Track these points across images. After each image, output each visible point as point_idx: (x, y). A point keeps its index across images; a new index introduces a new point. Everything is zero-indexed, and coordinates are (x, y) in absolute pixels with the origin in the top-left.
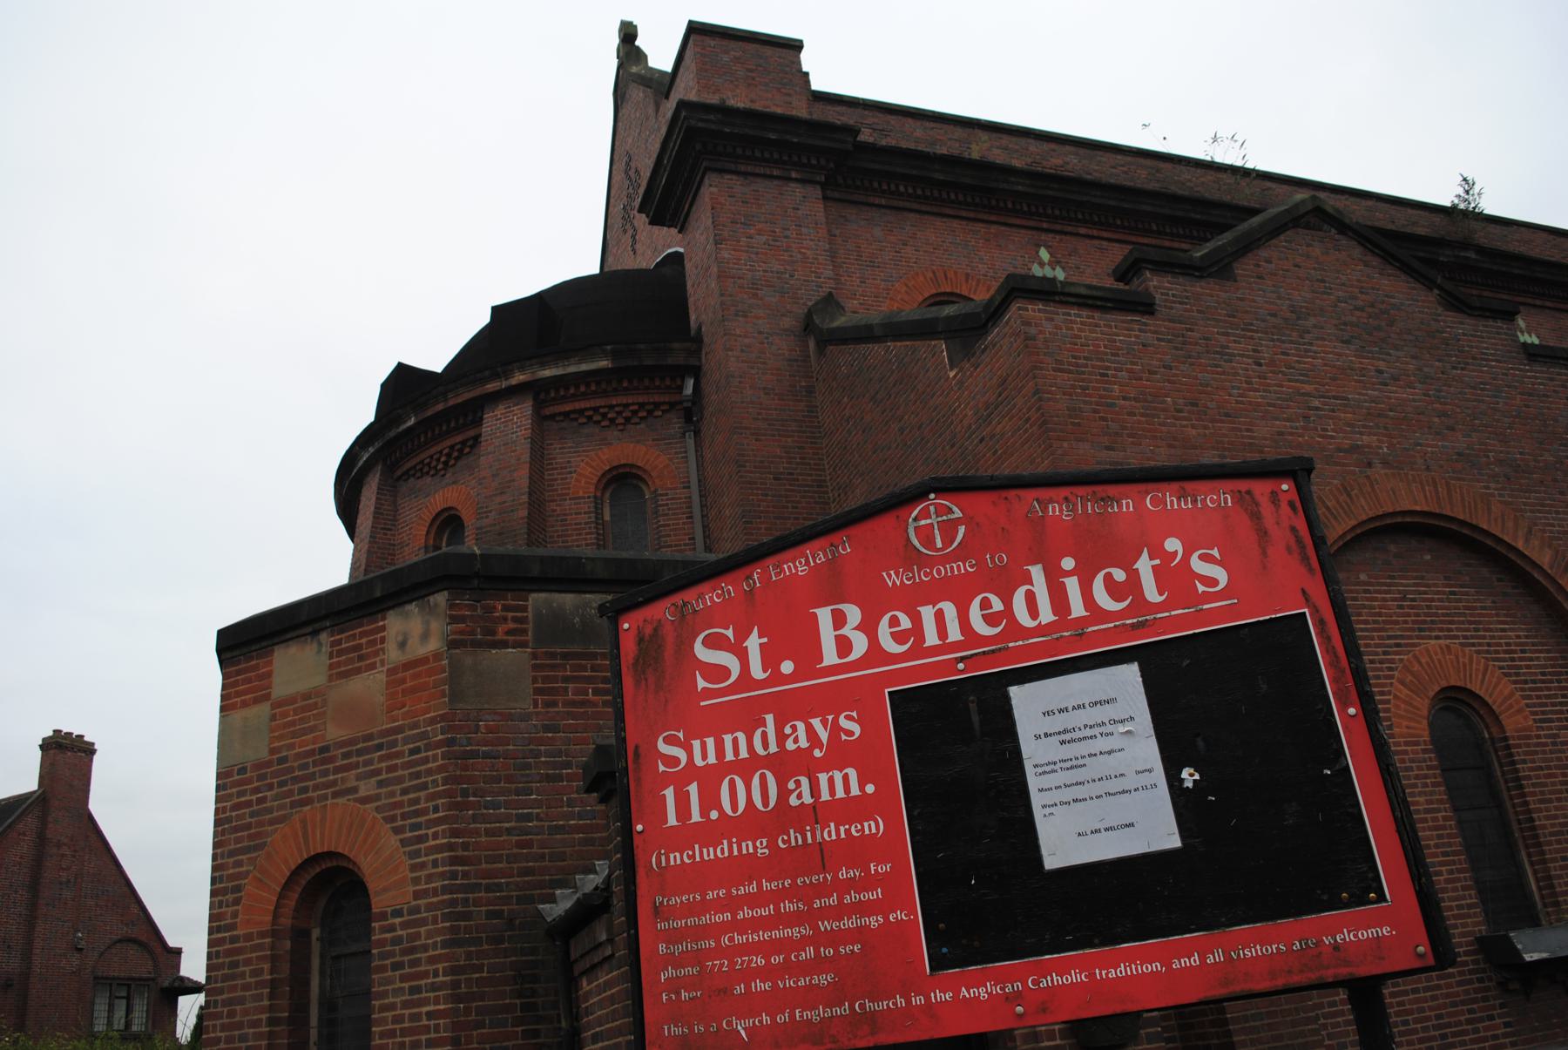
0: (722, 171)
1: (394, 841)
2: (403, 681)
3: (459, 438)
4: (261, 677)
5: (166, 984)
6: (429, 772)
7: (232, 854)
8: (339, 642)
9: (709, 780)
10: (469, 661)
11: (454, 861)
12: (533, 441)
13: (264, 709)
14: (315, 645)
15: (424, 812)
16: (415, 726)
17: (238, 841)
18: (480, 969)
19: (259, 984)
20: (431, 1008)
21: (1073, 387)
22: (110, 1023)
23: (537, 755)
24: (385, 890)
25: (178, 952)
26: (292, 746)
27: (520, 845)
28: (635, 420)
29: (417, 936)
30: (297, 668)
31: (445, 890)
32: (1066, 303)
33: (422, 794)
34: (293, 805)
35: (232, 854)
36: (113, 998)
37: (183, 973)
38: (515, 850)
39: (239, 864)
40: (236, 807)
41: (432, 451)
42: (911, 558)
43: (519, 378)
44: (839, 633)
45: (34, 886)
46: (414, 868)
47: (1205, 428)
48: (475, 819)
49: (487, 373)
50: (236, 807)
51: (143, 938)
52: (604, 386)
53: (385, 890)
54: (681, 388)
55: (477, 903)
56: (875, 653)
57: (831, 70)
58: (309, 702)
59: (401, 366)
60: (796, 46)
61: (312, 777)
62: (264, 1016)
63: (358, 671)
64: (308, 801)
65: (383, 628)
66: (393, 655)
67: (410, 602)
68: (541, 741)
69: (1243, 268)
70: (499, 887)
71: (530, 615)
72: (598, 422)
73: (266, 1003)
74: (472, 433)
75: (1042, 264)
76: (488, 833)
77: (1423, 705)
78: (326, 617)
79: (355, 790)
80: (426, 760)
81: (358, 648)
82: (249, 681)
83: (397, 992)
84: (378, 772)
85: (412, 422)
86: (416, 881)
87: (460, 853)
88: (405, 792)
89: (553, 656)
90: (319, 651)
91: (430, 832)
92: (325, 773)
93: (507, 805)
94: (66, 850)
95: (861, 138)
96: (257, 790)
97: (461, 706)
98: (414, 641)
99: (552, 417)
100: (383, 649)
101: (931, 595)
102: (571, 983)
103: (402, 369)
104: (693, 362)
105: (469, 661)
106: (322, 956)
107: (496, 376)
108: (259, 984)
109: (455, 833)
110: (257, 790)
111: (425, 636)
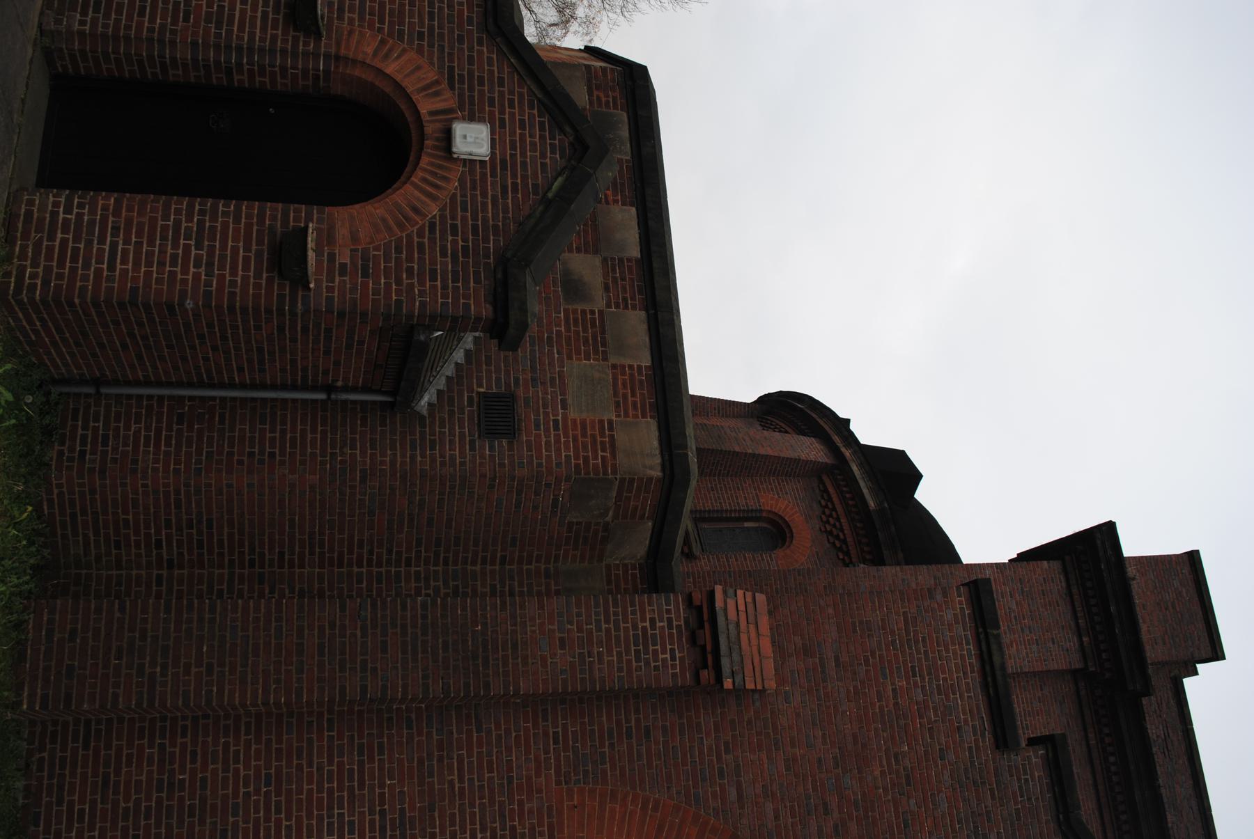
0: (1065, 572)
21: (892, 633)
32: (979, 642)
47: (885, 790)
57: (1204, 690)
60: (1215, 652)
72: (824, 513)
95: (1145, 701)
99: (821, 481)
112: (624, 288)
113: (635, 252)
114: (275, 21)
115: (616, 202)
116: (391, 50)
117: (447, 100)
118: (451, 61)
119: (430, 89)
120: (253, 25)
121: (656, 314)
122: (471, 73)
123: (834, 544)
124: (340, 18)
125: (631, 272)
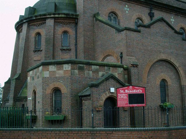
3: (41, 22)
4: (48, 68)
9: (121, 96)
11: (71, 90)
42: (129, 88)
44: (126, 91)
48: (73, 86)
56: (128, 92)
69: (152, 27)
75: (126, 8)
77: (160, 80)
99: (56, 22)
101: (130, 90)
113: (98, 67)
117: (107, 92)
119: (106, 94)
122: (103, 89)
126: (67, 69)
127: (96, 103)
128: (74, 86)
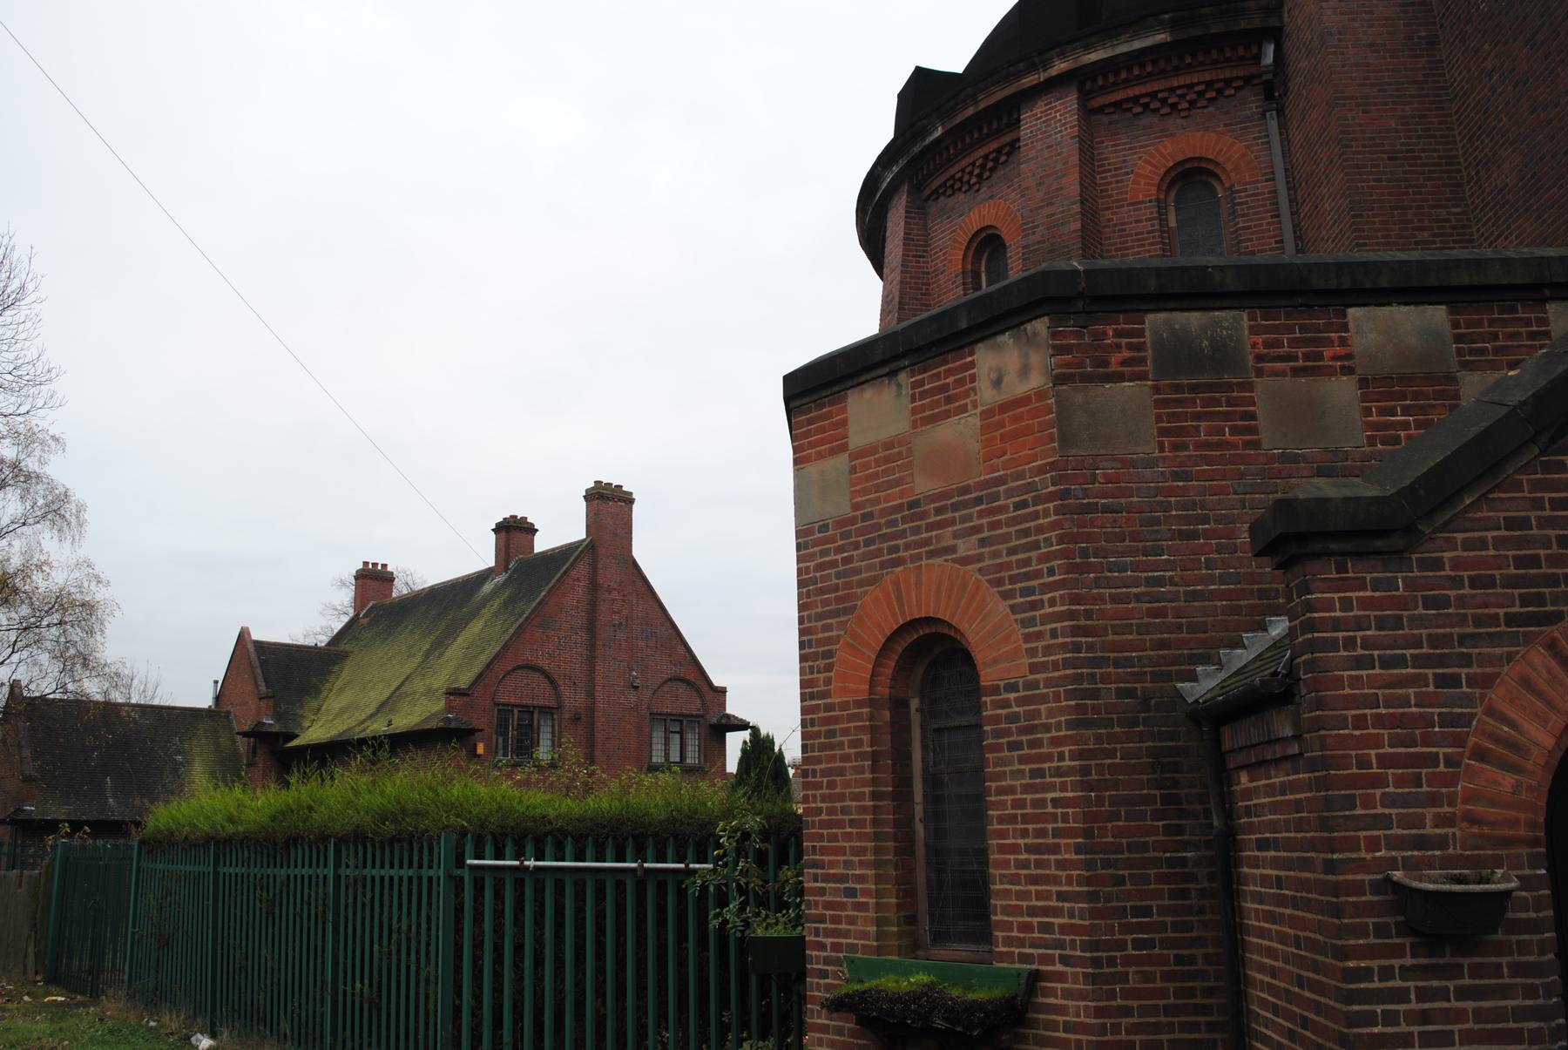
1: (1003, 607)
2: (1001, 424)
3: (994, 146)
5: (714, 721)
6: (1040, 529)
7: (820, 617)
8: (922, 383)
10: (1079, 398)
11: (1075, 631)
12: (1081, 142)
13: (841, 462)
14: (894, 387)
15: (1037, 574)
16: (1020, 476)
17: (825, 603)
18: (1111, 754)
19: (859, 756)
20: (1057, 794)
22: (667, 755)
23: (1167, 508)
24: (995, 661)
25: (723, 691)
26: (877, 501)
27: (1152, 613)
28: (1202, 103)
29: (1037, 714)
30: (875, 413)
31: (1067, 663)
33: (1033, 554)
34: (883, 565)
35: (820, 617)
36: (667, 732)
37: (729, 710)
38: (1146, 620)
39: (828, 628)
40: (820, 567)
41: (963, 163)
43: (1059, 67)
45: (591, 628)
46: (1028, 638)
48: (1097, 583)
49: (1021, 65)
50: (820, 567)
51: (691, 677)
52: (1162, 64)
53: (995, 661)
54: (1258, 58)
55: (1105, 679)
58: (892, 452)
59: (918, 69)
61: (902, 535)
62: (867, 790)
63: (947, 415)
64: (899, 562)
65: (972, 365)
66: (987, 394)
67: (1002, 332)
68: (1171, 492)
70: (1129, 662)
71: (1148, 339)
72: (1156, 110)
73: (868, 775)
74: (1008, 138)
76: (1115, 599)
78: (903, 355)
79: (953, 549)
80: (1036, 516)
81: (945, 388)
82: (822, 430)
83: (1016, 774)
84: (979, 529)
85: (939, 132)
86: (1032, 652)
87: (1083, 622)
88: (1012, 551)
89: (1178, 388)
90: (899, 394)
91: (1046, 597)
92: (917, 531)
93: (1135, 567)
94: (615, 595)
96: (840, 550)
97: (1074, 452)
98: (1011, 377)
99: (1100, 110)
100: (974, 389)
102: (1223, 776)
103: (921, 75)
104: (1273, 22)
105: (1079, 398)
106: (922, 727)
107: (1032, 68)
108: (859, 756)
109: (1076, 599)
110: (840, 550)
111: (1024, 372)
112: (1511, 336)
113: (1438, 315)
114: (1476, 971)
115: (1343, 342)
116: (1497, 739)
118: (1494, 621)
120: (1500, 1015)
121: (1551, 286)
122: (1512, 582)
123: (1210, 100)
124: (1441, 843)
125: (1479, 324)
126: (1022, 389)
127: (1388, 801)
128: (1110, 583)
